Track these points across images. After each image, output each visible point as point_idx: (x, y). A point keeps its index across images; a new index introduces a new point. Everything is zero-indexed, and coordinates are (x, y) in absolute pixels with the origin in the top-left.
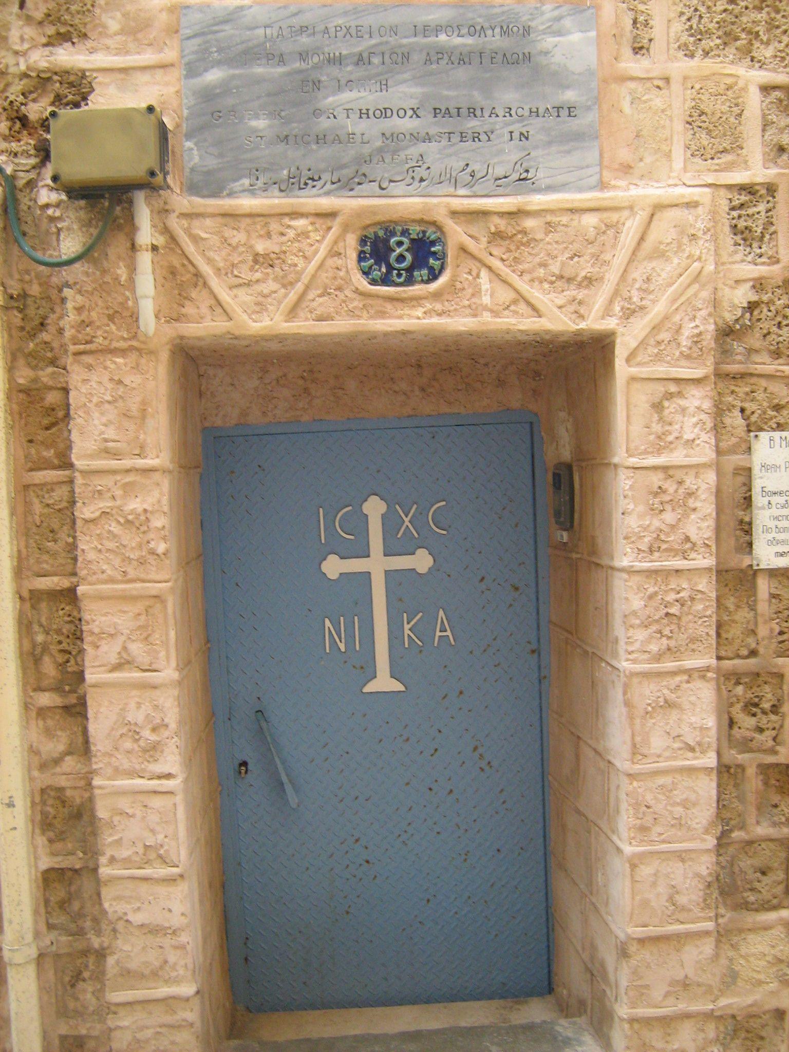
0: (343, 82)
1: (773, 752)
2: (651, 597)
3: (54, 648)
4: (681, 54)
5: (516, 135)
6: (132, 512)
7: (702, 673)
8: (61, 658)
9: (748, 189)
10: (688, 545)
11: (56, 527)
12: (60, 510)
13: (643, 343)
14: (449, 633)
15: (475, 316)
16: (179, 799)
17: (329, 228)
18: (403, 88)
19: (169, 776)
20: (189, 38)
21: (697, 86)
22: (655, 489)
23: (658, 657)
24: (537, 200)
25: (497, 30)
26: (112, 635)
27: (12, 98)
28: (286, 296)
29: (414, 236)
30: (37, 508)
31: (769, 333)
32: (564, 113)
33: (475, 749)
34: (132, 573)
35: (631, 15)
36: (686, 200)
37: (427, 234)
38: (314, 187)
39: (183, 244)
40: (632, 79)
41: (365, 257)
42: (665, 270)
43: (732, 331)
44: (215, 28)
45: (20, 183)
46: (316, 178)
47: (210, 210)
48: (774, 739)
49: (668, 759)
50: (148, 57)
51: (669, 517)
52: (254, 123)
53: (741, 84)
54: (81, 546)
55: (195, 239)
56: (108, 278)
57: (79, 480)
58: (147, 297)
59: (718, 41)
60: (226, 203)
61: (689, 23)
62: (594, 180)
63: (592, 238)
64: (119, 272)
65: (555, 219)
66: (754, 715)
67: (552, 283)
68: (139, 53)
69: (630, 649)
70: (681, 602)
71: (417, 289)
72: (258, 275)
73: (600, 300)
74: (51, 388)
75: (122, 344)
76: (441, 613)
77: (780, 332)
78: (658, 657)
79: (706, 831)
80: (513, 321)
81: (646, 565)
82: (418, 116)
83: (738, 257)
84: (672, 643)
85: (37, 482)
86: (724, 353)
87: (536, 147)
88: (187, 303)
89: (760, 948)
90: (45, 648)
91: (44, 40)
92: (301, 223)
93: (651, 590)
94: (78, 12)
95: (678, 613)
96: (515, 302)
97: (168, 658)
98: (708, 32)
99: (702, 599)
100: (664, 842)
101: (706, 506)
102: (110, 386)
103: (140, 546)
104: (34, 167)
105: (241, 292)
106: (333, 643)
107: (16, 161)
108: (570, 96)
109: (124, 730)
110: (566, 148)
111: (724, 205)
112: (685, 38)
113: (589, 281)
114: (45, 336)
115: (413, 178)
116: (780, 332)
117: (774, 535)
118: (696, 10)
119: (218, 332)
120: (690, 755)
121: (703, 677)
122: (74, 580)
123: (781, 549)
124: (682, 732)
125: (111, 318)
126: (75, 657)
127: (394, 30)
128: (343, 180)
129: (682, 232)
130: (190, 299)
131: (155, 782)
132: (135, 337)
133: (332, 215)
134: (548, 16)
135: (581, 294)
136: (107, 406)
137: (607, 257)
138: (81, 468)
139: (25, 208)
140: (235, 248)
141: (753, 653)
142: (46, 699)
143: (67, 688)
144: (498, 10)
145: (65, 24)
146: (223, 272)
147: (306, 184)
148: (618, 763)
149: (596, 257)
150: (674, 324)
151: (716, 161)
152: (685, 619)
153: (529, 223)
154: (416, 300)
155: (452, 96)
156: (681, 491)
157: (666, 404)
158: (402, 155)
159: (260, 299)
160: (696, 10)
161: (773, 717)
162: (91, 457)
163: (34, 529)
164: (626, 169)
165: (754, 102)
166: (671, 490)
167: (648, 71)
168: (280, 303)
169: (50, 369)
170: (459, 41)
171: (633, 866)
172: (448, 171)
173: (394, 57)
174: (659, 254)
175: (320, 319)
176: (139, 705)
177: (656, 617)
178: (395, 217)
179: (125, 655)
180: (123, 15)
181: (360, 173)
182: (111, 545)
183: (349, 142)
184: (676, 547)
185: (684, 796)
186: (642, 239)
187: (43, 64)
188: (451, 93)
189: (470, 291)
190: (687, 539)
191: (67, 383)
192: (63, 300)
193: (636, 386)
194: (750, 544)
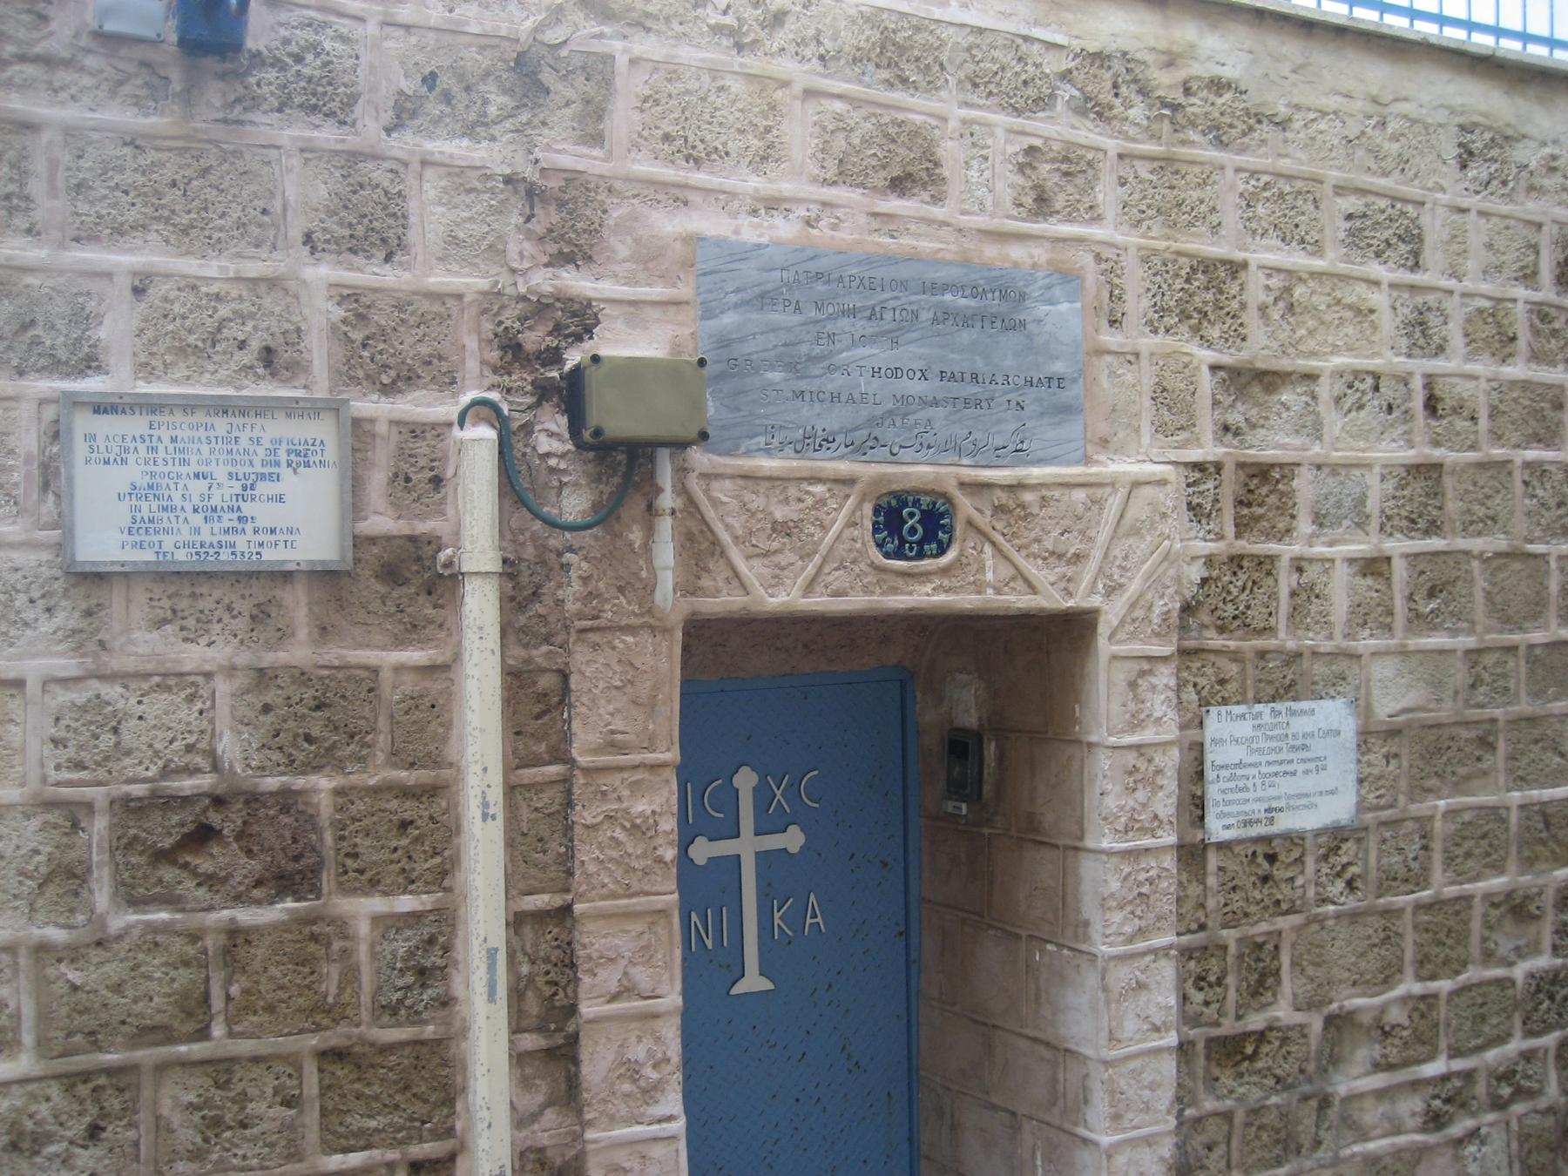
0: (857, 337)
1: (1217, 1024)
2: (1125, 878)
3: (540, 981)
4: (1147, 329)
6: (641, 814)
7: (1163, 952)
8: (548, 991)
9: (1198, 466)
11: (546, 834)
12: (549, 815)
13: (1122, 622)
14: (819, 919)
15: (979, 593)
16: (682, 1145)
17: (848, 496)
18: (912, 348)
19: (670, 1118)
20: (705, 274)
22: (1130, 768)
23: (1130, 939)
24: (1037, 473)
25: (997, 294)
26: (612, 960)
27: (508, 323)
28: (804, 569)
30: (525, 813)
32: (1055, 383)
33: (844, 1048)
34: (636, 887)
39: (703, 508)
40: (1109, 352)
42: (1142, 546)
44: (731, 266)
45: (515, 425)
47: (729, 471)
49: (1139, 1042)
50: (657, 291)
51: (1141, 795)
53: (1195, 362)
54: (581, 856)
55: (716, 503)
56: (619, 543)
57: (580, 780)
58: (666, 568)
60: (746, 463)
62: (1079, 454)
64: (632, 537)
65: (1049, 494)
66: (1201, 989)
68: (649, 285)
69: (1108, 932)
70: (1150, 881)
71: (927, 564)
72: (775, 545)
74: (545, 671)
75: (633, 621)
79: (1169, 1112)
80: (1012, 598)
83: (1193, 534)
85: (526, 782)
86: (1183, 628)
88: (704, 574)
90: (530, 979)
91: (545, 259)
92: (819, 489)
93: (1127, 870)
94: (585, 231)
96: (1013, 579)
97: (672, 979)
98: (1169, 310)
100: (1135, 1128)
101: (1170, 783)
102: (618, 668)
103: (644, 855)
105: (756, 562)
108: (1058, 367)
109: (622, 1070)
110: (1056, 420)
113: (1078, 558)
114: (538, 608)
119: (735, 607)
120: (1156, 1035)
121: (1167, 955)
122: (569, 897)
125: (621, 590)
126: (564, 989)
127: (903, 285)
128: (857, 443)
129: (1155, 510)
130: (708, 571)
131: (655, 1127)
132: (650, 611)
133: (849, 481)
134: (1040, 283)
136: (614, 692)
138: (585, 765)
139: (519, 455)
140: (753, 514)
141: (1202, 927)
142: (530, 1041)
143: (553, 1026)
144: (997, 273)
145: (569, 242)
148: (1087, 1051)
149: (1083, 532)
152: (1152, 898)
153: (1028, 497)
154: (925, 576)
155: (958, 362)
157: (1140, 681)
158: (912, 418)
159: (777, 571)
161: (1218, 990)
162: (597, 751)
163: (520, 839)
164: (1104, 442)
165: (1206, 382)
166: (1143, 769)
167: (1122, 345)
168: (796, 577)
169: (545, 648)
171: (1109, 1157)
174: (1135, 532)
175: (836, 594)
176: (639, 1039)
178: (908, 486)
179: (625, 982)
180: (635, 240)
182: (615, 854)
186: (1122, 516)
187: (547, 288)
188: (956, 356)
189: (975, 566)
190: (1156, 817)
191: (567, 664)
192: (566, 567)
193: (1117, 664)
194: (1202, 818)
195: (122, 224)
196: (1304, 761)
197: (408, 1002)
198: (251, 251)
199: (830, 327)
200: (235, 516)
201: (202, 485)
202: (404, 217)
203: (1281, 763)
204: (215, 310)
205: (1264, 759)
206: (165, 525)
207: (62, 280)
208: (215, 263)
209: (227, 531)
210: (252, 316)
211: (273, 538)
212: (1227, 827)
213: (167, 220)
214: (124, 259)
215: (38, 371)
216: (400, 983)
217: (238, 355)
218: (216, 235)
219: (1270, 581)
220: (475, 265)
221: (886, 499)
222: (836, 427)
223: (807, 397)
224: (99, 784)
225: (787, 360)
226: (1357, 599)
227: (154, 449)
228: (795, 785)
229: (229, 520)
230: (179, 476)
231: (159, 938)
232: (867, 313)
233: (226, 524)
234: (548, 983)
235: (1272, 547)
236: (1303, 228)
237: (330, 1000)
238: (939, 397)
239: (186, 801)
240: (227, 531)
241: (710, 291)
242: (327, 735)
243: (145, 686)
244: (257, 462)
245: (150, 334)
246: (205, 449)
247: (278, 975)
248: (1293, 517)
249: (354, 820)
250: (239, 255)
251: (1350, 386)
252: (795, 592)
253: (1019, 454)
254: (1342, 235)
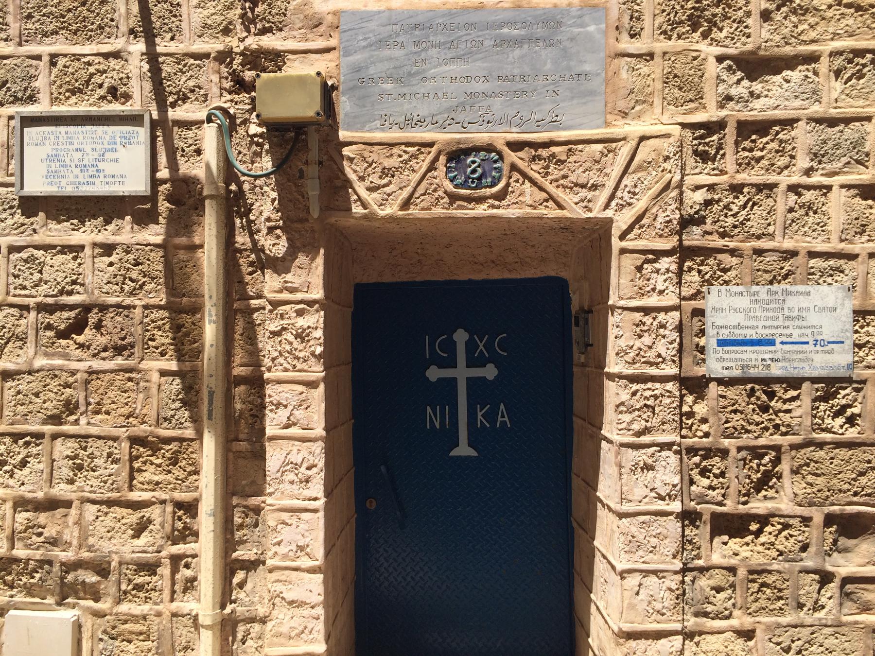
0: (440, 61)
1: (720, 504)
10: (660, 360)
14: (506, 419)
16: (321, 514)
17: (430, 153)
18: (478, 64)
19: (315, 499)
20: (345, 31)
21: (673, 58)
23: (639, 434)
27: (235, 67)
48: (724, 496)
51: (647, 340)
52: (384, 86)
53: (703, 56)
59: (688, 28)
63: (598, 159)
67: (571, 188)
70: (656, 397)
73: (603, 196)
76: (502, 406)
77: (726, 220)
78: (639, 434)
80: (545, 212)
84: (649, 425)
87: (563, 101)
89: (716, 646)
94: (277, 14)
95: (653, 405)
99: (669, 397)
100: (643, 562)
104: (247, 111)
107: (237, 107)
108: (587, 68)
110: (584, 101)
113: (595, 187)
116: (726, 220)
117: (721, 355)
118: (673, 8)
123: (726, 364)
124: (656, 486)
131: (307, 502)
135: (590, 195)
137: (607, 171)
150: (653, 214)
151: (684, 107)
156: (655, 323)
160: (673, 8)
166: (648, 323)
170: (516, 32)
173: (474, 43)
177: (638, 407)
184: (652, 360)
185: (658, 531)
187: (254, 46)
190: (659, 356)
195: (46, 32)
197: (176, 417)
198: (106, 40)
199: (423, 56)
200: (95, 169)
201: (80, 154)
202: (181, 16)
203: (777, 328)
204: (88, 69)
205: (760, 324)
206: (62, 174)
207: (19, 60)
208: (89, 47)
209: (91, 177)
210: (105, 71)
211: (113, 180)
213: (67, 29)
214: (45, 49)
215: (10, 103)
216: (173, 407)
217: (98, 91)
218: (90, 33)
219: (770, 202)
220: (217, 38)
224: (33, 297)
226: (854, 215)
227: (58, 138)
229: (92, 171)
230: (69, 150)
231: (56, 373)
233: (91, 173)
234: (251, 415)
237: (137, 411)
238: (497, 92)
239: (71, 307)
240: (91, 177)
241: (348, 41)
242: (140, 278)
243: (54, 251)
244: (106, 143)
245: (58, 83)
246: (81, 137)
247: (112, 396)
248: (792, 157)
249: (153, 321)
250: (99, 43)
252: (396, 207)
253: (555, 124)
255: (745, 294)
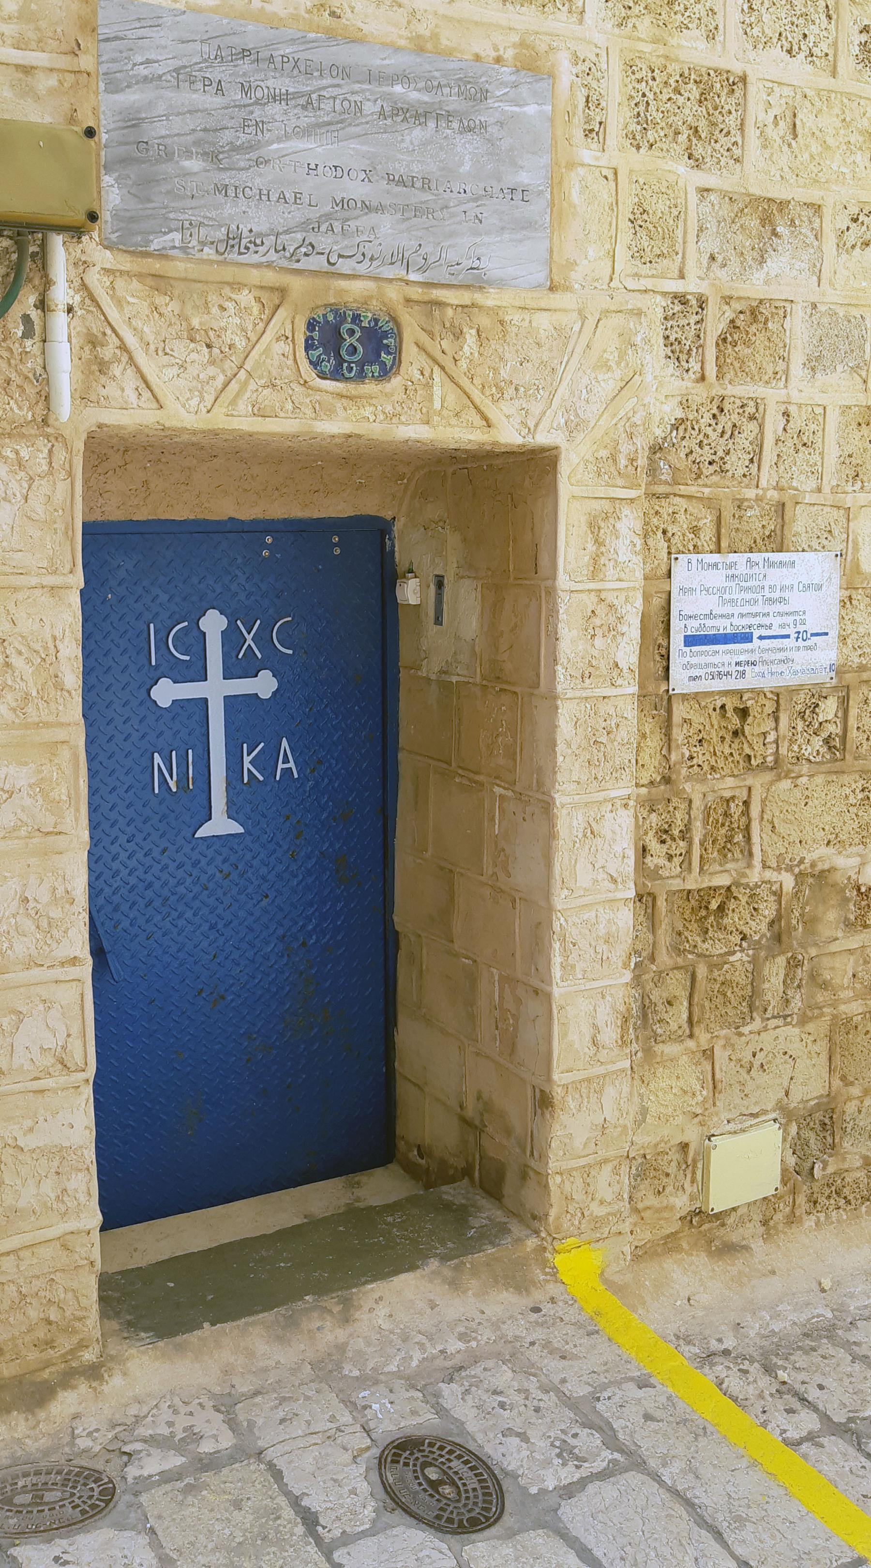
5: (471, 214)
9: (681, 299)
14: (291, 764)
18: (353, 145)
20: (107, 40)
21: (641, 181)
29: (365, 324)
31: (691, 452)
32: (518, 196)
35: (585, 92)
36: (630, 307)
37: (380, 324)
38: (256, 252)
41: (313, 345)
43: (660, 448)
46: (258, 241)
61: (637, 110)
66: (663, 842)
71: (369, 387)
76: (285, 743)
79: (626, 966)
81: (578, 694)
82: (370, 181)
106: (163, 782)
108: (524, 178)
111: (660, 314)
112: (633, 127)
115: (363, 255)
117: (688, 659)
118: (644, 95)
121: (626, 806)
127: (344, 72)
146: (152, 347)
147: (247, 248)
158: (353, 224)
161: (682, 843)
170: (414, 95)
172: (401, 250)
181: (307, 242)
183: (295, 203)
196: (780, 614)
199: (257, 113)
203: (756, 615)
205: (737, 611)
212: (694, 679)
221: (321, 312)
222: (264, 228)
223: (231, 193)
225: (208, 148)
228: (267, 628)
232: (302, 101)
235: (759, 390)
236: (811, 38)
241: (114, 61)
251: (855, 220)
254: (856, 50)
255: (720, 566)
